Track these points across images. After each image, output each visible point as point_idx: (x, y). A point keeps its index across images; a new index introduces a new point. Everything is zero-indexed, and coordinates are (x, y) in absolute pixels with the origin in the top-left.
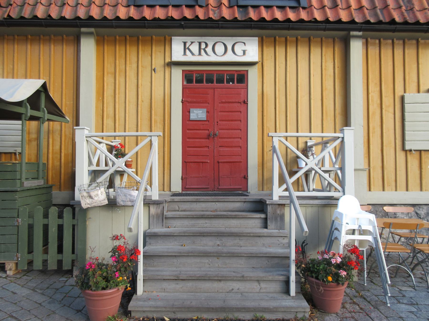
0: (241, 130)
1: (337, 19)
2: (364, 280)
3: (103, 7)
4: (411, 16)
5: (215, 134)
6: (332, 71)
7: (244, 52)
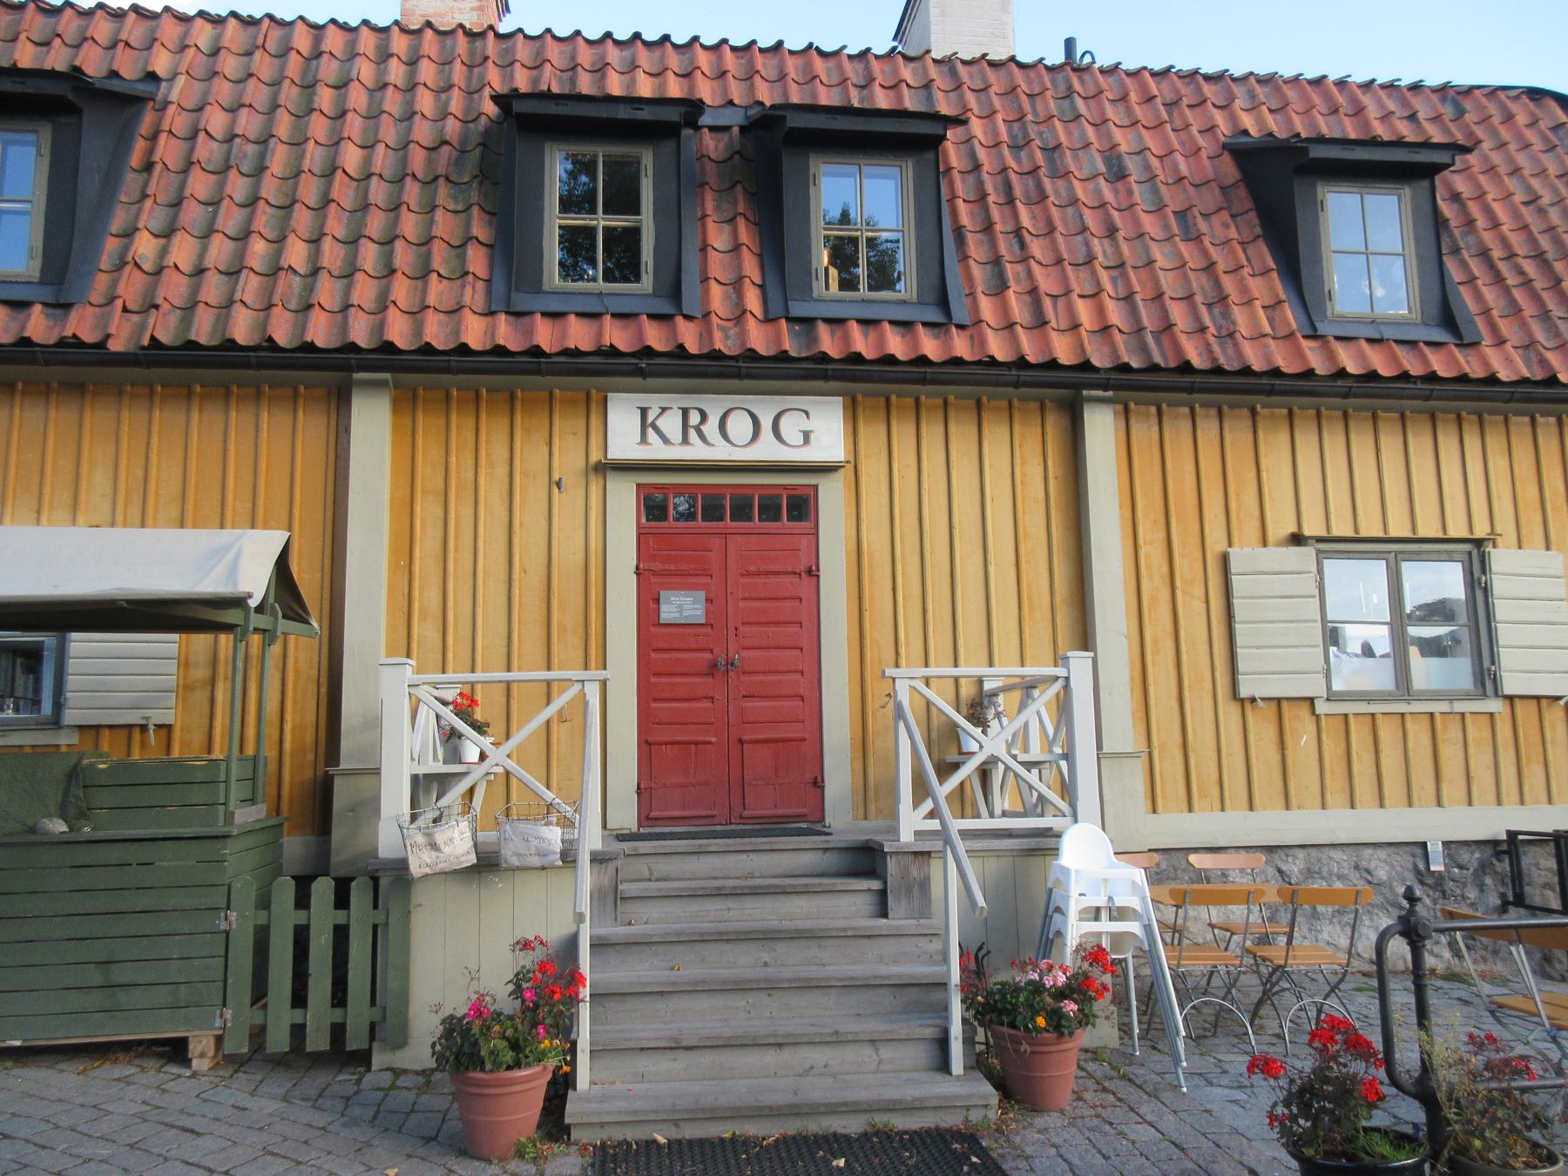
0: (801, 649)
1: (1046, 359)
2: (1133, 1046)
3: (419, 316)
4: (1230, 352)
5: (730, 663)
6: (1041, 487)
7: (807, 436)
